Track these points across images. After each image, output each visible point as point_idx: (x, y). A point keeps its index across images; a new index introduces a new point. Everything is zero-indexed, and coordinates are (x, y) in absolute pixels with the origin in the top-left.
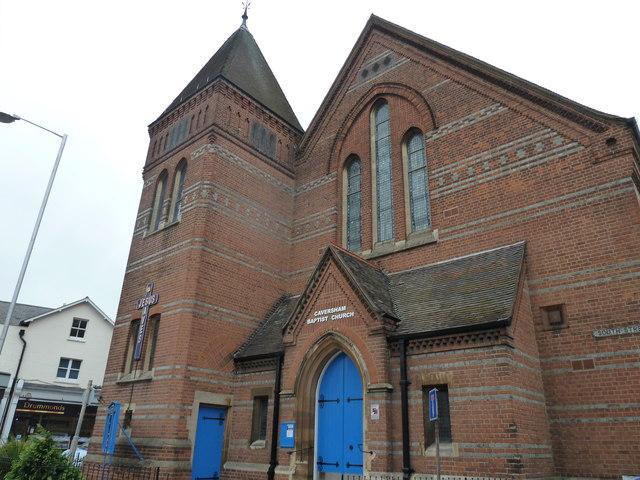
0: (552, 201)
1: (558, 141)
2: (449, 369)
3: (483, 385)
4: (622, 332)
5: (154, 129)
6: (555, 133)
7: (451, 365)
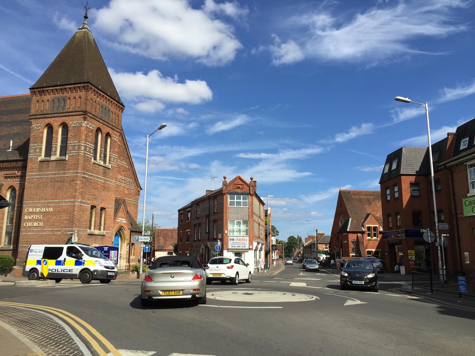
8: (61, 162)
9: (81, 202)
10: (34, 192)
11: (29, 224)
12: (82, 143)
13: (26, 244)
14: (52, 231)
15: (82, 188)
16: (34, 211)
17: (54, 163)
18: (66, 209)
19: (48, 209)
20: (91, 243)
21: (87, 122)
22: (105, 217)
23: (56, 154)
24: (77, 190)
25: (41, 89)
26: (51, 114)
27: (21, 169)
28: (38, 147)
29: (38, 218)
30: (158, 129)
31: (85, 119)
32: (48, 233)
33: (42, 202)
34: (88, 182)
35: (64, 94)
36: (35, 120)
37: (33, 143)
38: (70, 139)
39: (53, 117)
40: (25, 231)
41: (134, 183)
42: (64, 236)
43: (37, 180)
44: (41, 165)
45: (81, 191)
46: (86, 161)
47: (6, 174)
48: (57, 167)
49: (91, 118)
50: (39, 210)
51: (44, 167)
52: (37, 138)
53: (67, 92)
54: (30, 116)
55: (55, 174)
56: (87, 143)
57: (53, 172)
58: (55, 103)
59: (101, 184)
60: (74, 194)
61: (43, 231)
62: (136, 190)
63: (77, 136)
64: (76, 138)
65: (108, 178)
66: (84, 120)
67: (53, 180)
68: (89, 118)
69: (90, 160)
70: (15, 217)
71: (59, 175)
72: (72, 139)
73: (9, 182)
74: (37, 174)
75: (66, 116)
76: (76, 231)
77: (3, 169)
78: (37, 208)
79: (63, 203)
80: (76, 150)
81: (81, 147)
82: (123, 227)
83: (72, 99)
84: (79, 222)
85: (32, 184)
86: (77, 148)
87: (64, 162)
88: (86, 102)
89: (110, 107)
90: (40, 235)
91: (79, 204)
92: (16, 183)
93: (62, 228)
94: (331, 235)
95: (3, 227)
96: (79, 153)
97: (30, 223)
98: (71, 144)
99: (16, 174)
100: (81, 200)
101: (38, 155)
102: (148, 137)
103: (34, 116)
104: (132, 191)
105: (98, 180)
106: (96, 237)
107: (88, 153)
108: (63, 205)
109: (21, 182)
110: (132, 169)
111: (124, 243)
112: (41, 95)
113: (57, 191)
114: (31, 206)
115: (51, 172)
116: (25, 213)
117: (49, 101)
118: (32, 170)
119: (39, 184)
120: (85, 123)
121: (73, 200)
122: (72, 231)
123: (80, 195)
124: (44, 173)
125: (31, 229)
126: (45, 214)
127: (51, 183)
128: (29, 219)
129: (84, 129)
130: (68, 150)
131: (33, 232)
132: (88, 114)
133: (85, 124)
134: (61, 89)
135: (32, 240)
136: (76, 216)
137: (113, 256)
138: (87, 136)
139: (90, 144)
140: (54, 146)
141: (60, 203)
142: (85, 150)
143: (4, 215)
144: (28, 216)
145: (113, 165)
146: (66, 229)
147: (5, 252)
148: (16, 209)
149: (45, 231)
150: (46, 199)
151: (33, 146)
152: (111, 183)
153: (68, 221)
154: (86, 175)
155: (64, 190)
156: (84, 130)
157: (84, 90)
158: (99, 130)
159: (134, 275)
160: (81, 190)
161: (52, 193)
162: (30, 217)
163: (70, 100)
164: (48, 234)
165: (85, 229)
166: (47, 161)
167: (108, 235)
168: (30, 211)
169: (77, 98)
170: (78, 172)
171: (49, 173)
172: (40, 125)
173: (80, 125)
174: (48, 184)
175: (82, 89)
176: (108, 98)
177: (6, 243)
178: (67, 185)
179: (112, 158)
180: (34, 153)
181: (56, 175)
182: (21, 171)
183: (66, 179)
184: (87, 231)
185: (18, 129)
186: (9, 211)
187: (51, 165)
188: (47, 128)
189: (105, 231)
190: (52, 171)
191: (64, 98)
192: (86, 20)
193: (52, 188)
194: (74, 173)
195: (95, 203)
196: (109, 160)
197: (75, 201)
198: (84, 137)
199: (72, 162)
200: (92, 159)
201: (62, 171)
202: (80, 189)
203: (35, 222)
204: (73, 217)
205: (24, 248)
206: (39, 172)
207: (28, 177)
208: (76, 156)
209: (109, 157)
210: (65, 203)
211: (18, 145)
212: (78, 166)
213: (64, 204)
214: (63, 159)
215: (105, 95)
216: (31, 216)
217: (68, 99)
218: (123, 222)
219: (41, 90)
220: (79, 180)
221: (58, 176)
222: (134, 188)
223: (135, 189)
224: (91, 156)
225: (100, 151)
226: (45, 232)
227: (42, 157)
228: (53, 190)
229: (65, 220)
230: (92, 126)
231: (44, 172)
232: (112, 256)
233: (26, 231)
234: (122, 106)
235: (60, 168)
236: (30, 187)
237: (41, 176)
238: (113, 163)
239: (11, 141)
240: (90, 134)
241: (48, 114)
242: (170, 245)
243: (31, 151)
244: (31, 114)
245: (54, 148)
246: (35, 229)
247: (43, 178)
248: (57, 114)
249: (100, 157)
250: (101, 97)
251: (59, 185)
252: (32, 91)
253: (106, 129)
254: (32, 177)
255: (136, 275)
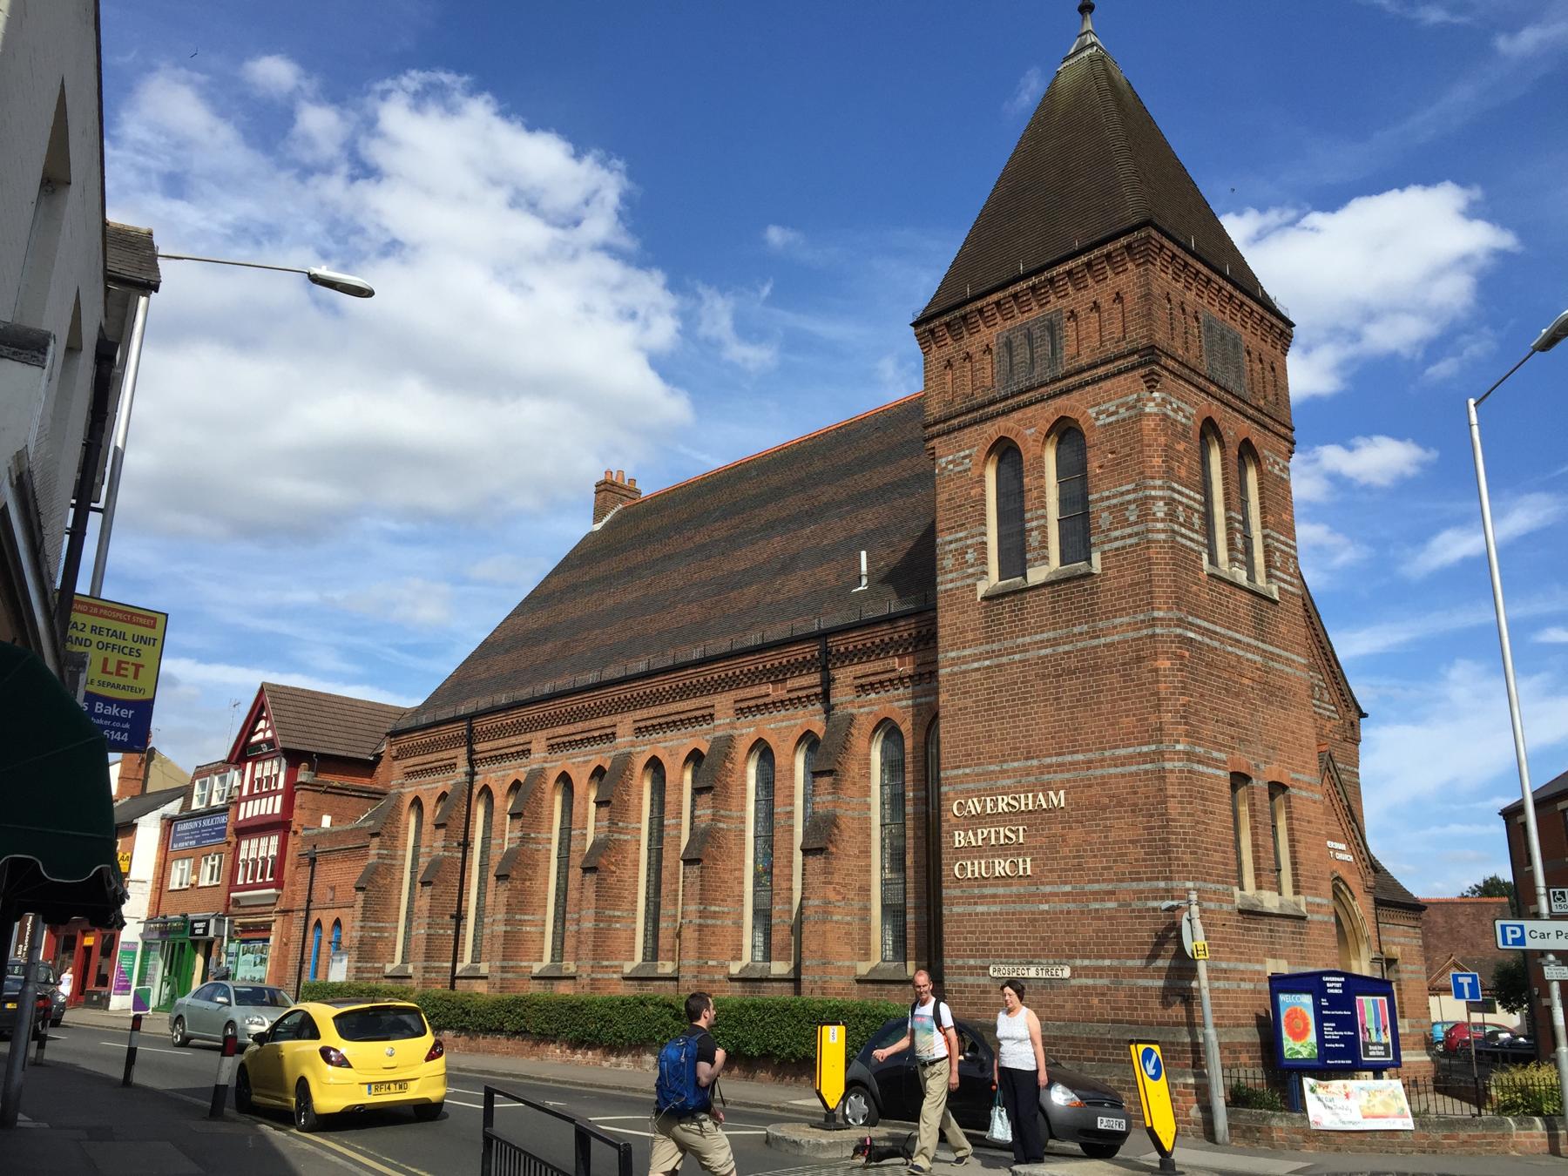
8: (1074, 587)
9: (1189, 756)
10: (979, 728)
11: (976, 868)
12: (1154, 488)
13: (974, 957)
14: (1078, 894)
15: (1184, 689)
16: (989, 811)
17: (1044, 594)
18: (1127, 794)
19: (1047, 797)
20: (1257, 954)
21: (1164, 395)
22: (1291, 830)
23: (1045, 558)
24: (1165, 699)
25: (957, 313)
26: (1006, 398)
27: (910, 650)
28: (969, 542)
29: (1010, 839)
30: (1535, 349)
31: (1154, 383)
32: (1058, 908)
33: (1015, 770)
34: (1203, 661)
35: (1048, 306)
36: (945, 438)
37: (948, 529)
38: (1100, 480)
39: (1013, 410)
40: (961, 898)
41: (1331, 690)
42: (1137, 917)
43: (985, 679)
44: (993, 611)
45: (1184, 705)
46: (1180, 566)
47: (859, 674)
48: (1058, 612)
49: (1175, 374)
50: (1008, 804)
51: (1005, 618)
52: (964, 505)
53: (1059, 295)
54: (926, 427)
55: (1054, 643)
56: (1176, 485)
57: (1045, 636)
58: (1015, 353)
59: (1252, 672)
60: (1153, 719)
61: (1038, 895)
62: (1341, 722)
63: (1128, 461)
64: (1127, 472)
65: (1277, 646)
66: (1149, 387)
67: (1047, 668)
68: (1167, 377)
69: (1195, 562)
70: (910, 843)
71: (1072, 642)
72: (1106, 478)
73: (874, 704)
74: (981, 654)
75: (1068, 391)
76: (1194, 896)
77: (846, 657)
78: (1000, 798)
79: (1110, 766)
80: (1130, 525)
81: (1154, 504)
82: (1344, 883)
83: (1082, 315)
84: (1196, 853)
85: (965, 698)
86: (1137, 512)
87: (1087, 584)
88: (1150, 309)
89: (1239, 329)
90: (1027, 913)
91: (1181, 764)
92: (898, 705)
93: (1122, 881)
95: (870, 886)
96: (1148, 531)
97: (980, 863)
98: (1106, 503)
99: (894, 670)
100: (1188, 748)
101: (973, 575)
102: (1472, 409)
103: (942, 425)
104: (1329, 725)
105: (1241, 653)
106: (1270, 925)
107: (1183, 530)
108: (1110, 776)
109: (919, 700)
110: (1315, 629)
111: (1355, 959)
112: (958, 338)
113: (1073, 713)
114: (973, 791)
115: (1038, 637)
116: (954, 821)
117: (991, 353)
118: (958, 638)
119: (995, 692)
120: (1154, 400)
121: (1153, 747)
122: (1169, 893)
123: (1180, 723)
124: (1007, 644)
125: (988, 891)
126: (1036, 818)
127: (1045, 684)
128: (974, 844)
129: (1153, 426)
130: (1095, 528)
131: (995, 903)
132: (1163, 360)
133: (1157, 405)
134: (1033, 288)
135: (996, 938)
136: (1174, 820)
137: (1371, 1025)
138: (1169, 454)
139: (1187, 491)
140: (1034, 524)
141: (1096, 768)
142: (1171, 516)
143: (869, 835)
144: (966, 831)
145: (1286, 586)
146: (1143, 885)
147: (889, 991)
148: (909, 809)
149: (1046, 898)
150: (1029, 752)
151: (951, 542)
152: (1288, 669)
153: (1142, 847)
154: (1191, 630)
155: (1106, 708)
156: (1154, 430)
157: (1133, 260)
158: (1209, 429)
159: (1532, 1137)
160: (1184, 699)
161: (1054, 727)
162: (975, 835)
163: (1075, 320)
164: (1062, 912)
165: (1225, 886)
166: (1015, 592)
167: (1316, 917)
168: (974, 813)
169: (1105, 305)
170: (1154, 619)
171: (1028, 639)
172: (967, 452)
173: (1133, 412)
174: (1032, 686)
175: (1121, 260)
176: (1229, 287)
177: (889, 954)
178: (1111, 684)
179: (1278, 554)
180: (956, 570)
181: (1059, 644)
182: (911, 658)
183: (1106, 657)
184: (1233, 894)
185: (877, 515)
186: (887, 821)
187: (1031, 607)
188: (994, 459)
189: (1302, 899)
190: (1041, 629)
191: (1050, 320)
192: (1088, 16)
193: (1052, 705)
194: (1136, 626)
195: (1244, 760)
196: (1266, 562)
197: (1161, 753)
198: (1157, 461)
199: (1123, 576)
200: (1201, 560)
201: (1080, 624)
202: (1174, 694)
203: (999, 856)
204: (1165, 827)
205: (966, 975)
206: (987, 643)
207: (948, 670)
208: (1135, 551)
209: (1265, 552)
210: (1116, 766)
211: (887, 566)
212: (1150, 592)
213: (1112, 771)
214: (1079, 572)
215: (1214, 277)
216: (979, 831)
217: (1069, 319)
218: (1340, 856)
219: (956, 318)
220: (1167, 652)
221: (1067, 648)
222: (1333, 711)
223: (1338, 717)
224: (1197, 542)
225: (1227, 525)
226: (1047, 902)
227: (992, 579)
228: (1056, 710)
229: (1130, 842)
230: (1182, 411)
231: (1005, 639)
232: (1367, 1026)
233: (967, 898)
234: (1281, 325)
235: (1073, 614)
236: (960, 709)
237: (996, 656)
238: (1285, 577)
239: (863, 554)
240: (1181, 447)
241: (992, 402)
242: (1449, 968)
243: (945, 562)
244: (930, 419)
245: (1034, 533)
246: (1001, 891)
247: (1008, 664)
248: (1031, 394)
249: (1229, 550)
250: (1200, 287)
251: (1078, 689)
252: (924, 332)
253: (1236, 427)
254: (964, 667)
255: (1543, 1136)
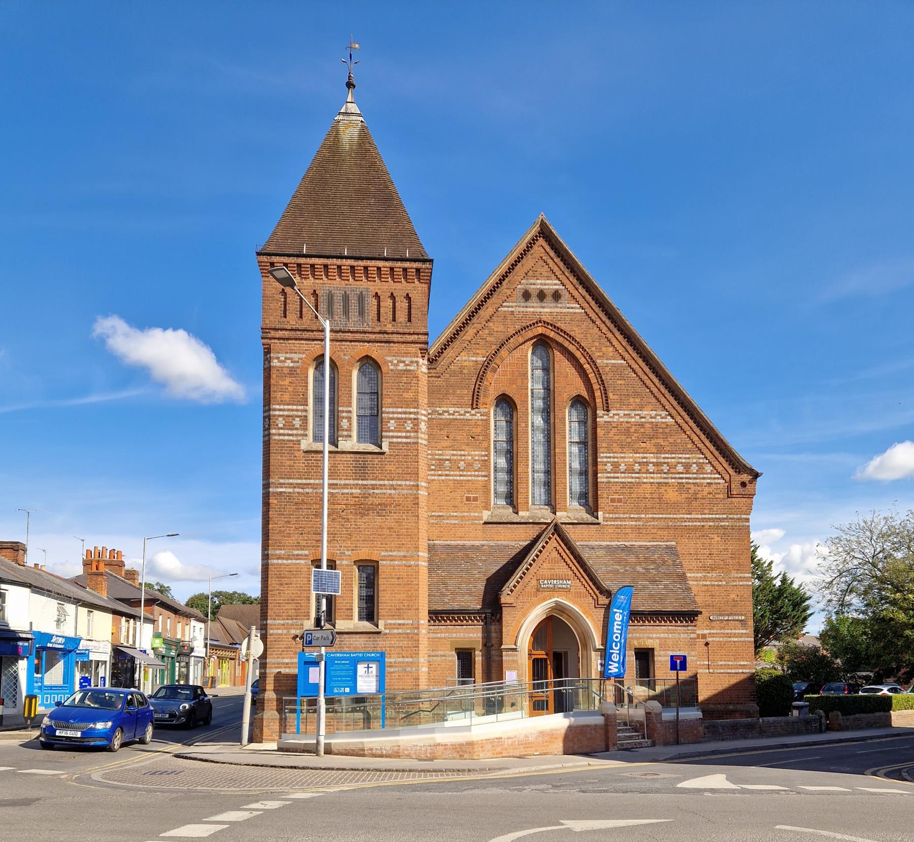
0: (696, 516)
1: (709, 468)
2: (656, 638)
3: (679, 650)
4: (726, 618)
5: (489, 580)
6: (707, 461)
7: (658, 635)
94: (335, 623)
222: (718, 478)
245: (345, 421)
